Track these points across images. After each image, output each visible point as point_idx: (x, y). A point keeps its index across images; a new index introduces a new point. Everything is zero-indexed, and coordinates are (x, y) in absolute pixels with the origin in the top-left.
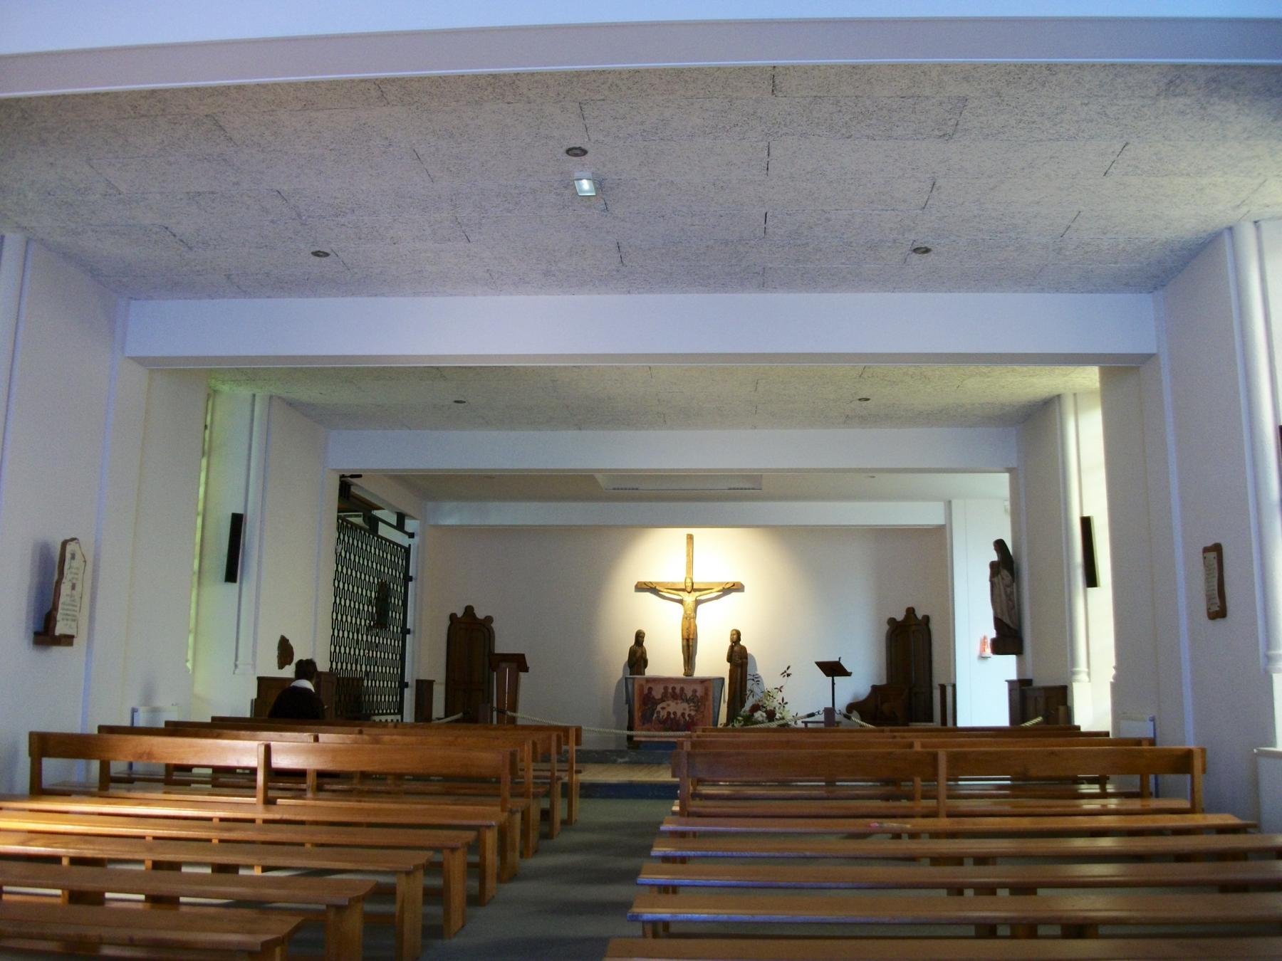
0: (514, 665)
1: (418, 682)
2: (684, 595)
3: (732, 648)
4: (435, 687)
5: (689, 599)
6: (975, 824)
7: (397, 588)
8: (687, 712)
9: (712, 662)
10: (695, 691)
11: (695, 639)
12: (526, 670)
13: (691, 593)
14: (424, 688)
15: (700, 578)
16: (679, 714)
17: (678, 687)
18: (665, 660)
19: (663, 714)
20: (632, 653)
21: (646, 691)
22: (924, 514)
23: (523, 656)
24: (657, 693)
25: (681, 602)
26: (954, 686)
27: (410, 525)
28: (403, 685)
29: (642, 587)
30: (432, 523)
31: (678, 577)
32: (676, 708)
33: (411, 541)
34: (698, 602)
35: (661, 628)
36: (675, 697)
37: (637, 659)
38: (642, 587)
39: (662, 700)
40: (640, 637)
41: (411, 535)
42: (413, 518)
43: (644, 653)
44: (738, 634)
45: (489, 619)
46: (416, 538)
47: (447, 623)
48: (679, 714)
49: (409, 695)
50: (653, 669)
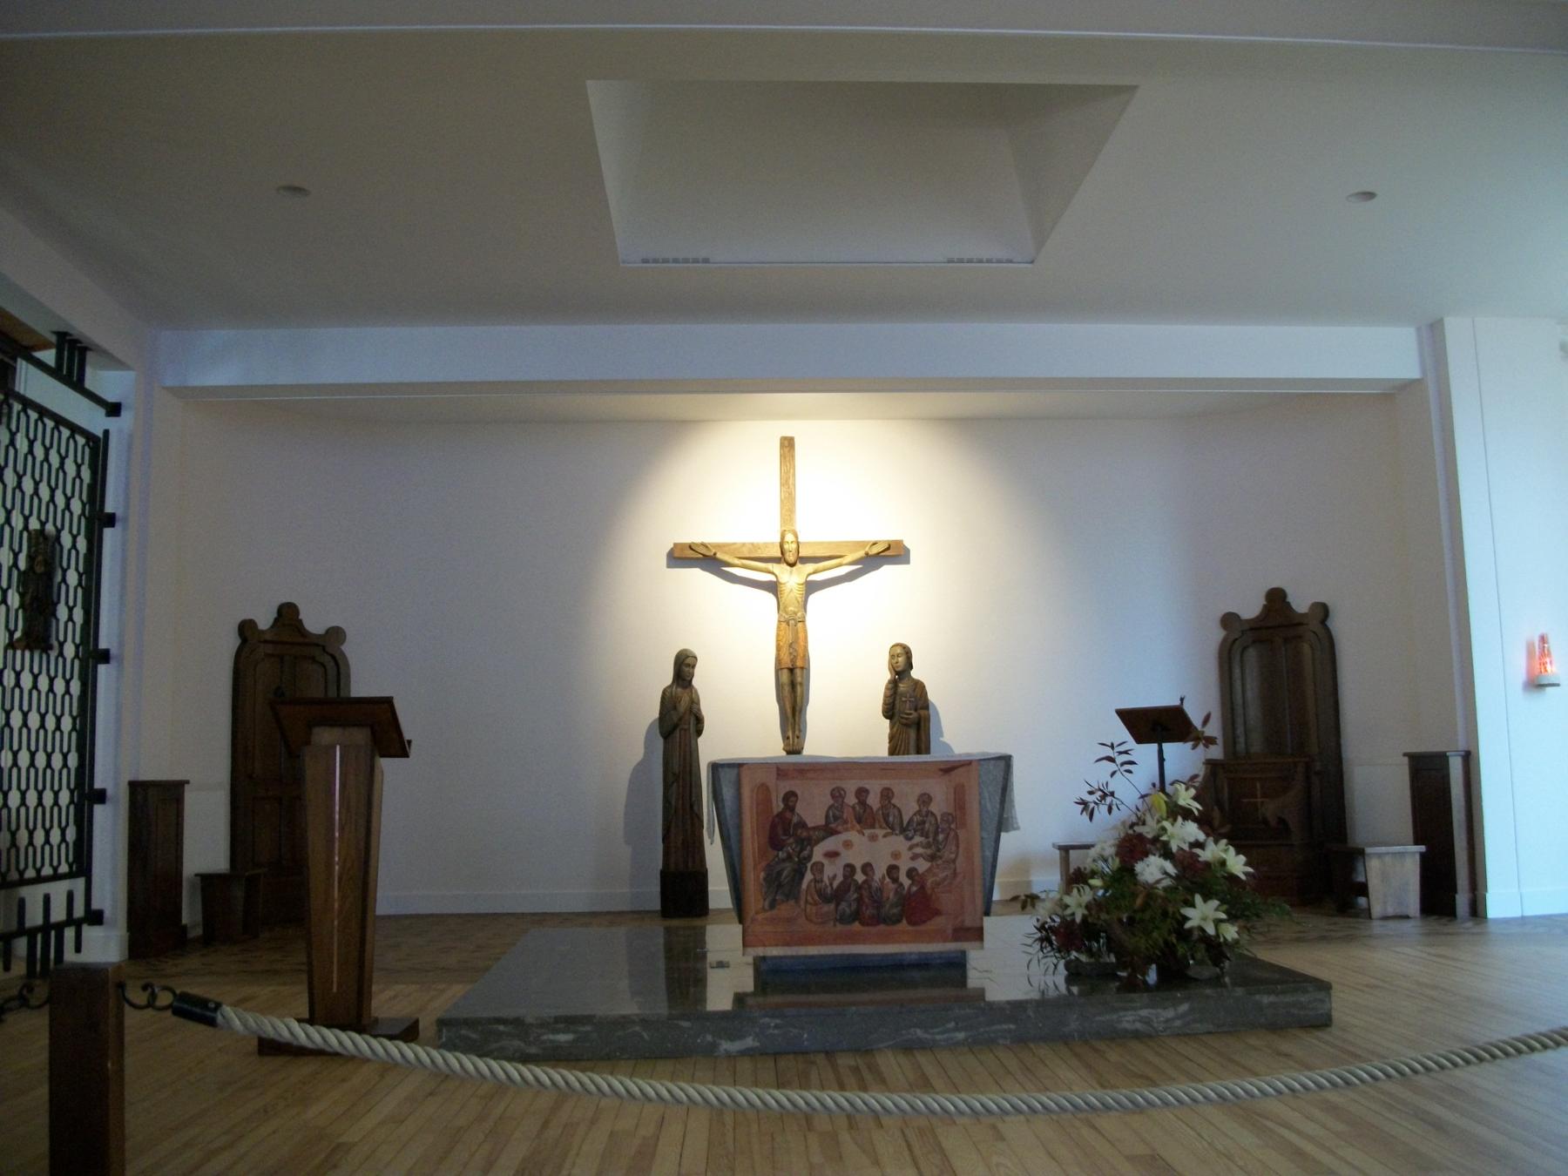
0: (360, 736)
1: (134, 785)
2: (782, 573)
3: (893, 685)
4: (190, 798)
5: (792, 579)
6: (711, 836)
7: (72, 542)
8: (904, 865)
9: (845, 721)
10: (925, 799)
11: (805, 669)
12: (400, 749)
13: (790, 569)
14: (156, 806)
15: (813, 531)
16: (880, 871)
17: (875, 787)
18: (739, 724)
19: (833, 872)
20: (669, 703)
21: (778, 806)
22: (1378, 353)
23: (388, 701)
24: (812, 811)
25: (773, 588)
26: (1470, 760)
27: (100, 379)
28: (88, 796)
29: (683, 557)
30: (169, 383)
31: (763, 532)
32: (872, 852)
33: (112, 424)
34: (811, 587)
35: (732, 646)
36: (865, 818)
37: (680, 718)
38: (683, 557)
39: (828, 831)
40: (684, 666)
41: (114, 410)
42: (119, 364)
43: (694, 702)
44: (908, 653)
45: (336, 634)
46: (126, 419)
47: (233, 642)
48: (880, 871)
49: (110, 826)
50: (711, 748)
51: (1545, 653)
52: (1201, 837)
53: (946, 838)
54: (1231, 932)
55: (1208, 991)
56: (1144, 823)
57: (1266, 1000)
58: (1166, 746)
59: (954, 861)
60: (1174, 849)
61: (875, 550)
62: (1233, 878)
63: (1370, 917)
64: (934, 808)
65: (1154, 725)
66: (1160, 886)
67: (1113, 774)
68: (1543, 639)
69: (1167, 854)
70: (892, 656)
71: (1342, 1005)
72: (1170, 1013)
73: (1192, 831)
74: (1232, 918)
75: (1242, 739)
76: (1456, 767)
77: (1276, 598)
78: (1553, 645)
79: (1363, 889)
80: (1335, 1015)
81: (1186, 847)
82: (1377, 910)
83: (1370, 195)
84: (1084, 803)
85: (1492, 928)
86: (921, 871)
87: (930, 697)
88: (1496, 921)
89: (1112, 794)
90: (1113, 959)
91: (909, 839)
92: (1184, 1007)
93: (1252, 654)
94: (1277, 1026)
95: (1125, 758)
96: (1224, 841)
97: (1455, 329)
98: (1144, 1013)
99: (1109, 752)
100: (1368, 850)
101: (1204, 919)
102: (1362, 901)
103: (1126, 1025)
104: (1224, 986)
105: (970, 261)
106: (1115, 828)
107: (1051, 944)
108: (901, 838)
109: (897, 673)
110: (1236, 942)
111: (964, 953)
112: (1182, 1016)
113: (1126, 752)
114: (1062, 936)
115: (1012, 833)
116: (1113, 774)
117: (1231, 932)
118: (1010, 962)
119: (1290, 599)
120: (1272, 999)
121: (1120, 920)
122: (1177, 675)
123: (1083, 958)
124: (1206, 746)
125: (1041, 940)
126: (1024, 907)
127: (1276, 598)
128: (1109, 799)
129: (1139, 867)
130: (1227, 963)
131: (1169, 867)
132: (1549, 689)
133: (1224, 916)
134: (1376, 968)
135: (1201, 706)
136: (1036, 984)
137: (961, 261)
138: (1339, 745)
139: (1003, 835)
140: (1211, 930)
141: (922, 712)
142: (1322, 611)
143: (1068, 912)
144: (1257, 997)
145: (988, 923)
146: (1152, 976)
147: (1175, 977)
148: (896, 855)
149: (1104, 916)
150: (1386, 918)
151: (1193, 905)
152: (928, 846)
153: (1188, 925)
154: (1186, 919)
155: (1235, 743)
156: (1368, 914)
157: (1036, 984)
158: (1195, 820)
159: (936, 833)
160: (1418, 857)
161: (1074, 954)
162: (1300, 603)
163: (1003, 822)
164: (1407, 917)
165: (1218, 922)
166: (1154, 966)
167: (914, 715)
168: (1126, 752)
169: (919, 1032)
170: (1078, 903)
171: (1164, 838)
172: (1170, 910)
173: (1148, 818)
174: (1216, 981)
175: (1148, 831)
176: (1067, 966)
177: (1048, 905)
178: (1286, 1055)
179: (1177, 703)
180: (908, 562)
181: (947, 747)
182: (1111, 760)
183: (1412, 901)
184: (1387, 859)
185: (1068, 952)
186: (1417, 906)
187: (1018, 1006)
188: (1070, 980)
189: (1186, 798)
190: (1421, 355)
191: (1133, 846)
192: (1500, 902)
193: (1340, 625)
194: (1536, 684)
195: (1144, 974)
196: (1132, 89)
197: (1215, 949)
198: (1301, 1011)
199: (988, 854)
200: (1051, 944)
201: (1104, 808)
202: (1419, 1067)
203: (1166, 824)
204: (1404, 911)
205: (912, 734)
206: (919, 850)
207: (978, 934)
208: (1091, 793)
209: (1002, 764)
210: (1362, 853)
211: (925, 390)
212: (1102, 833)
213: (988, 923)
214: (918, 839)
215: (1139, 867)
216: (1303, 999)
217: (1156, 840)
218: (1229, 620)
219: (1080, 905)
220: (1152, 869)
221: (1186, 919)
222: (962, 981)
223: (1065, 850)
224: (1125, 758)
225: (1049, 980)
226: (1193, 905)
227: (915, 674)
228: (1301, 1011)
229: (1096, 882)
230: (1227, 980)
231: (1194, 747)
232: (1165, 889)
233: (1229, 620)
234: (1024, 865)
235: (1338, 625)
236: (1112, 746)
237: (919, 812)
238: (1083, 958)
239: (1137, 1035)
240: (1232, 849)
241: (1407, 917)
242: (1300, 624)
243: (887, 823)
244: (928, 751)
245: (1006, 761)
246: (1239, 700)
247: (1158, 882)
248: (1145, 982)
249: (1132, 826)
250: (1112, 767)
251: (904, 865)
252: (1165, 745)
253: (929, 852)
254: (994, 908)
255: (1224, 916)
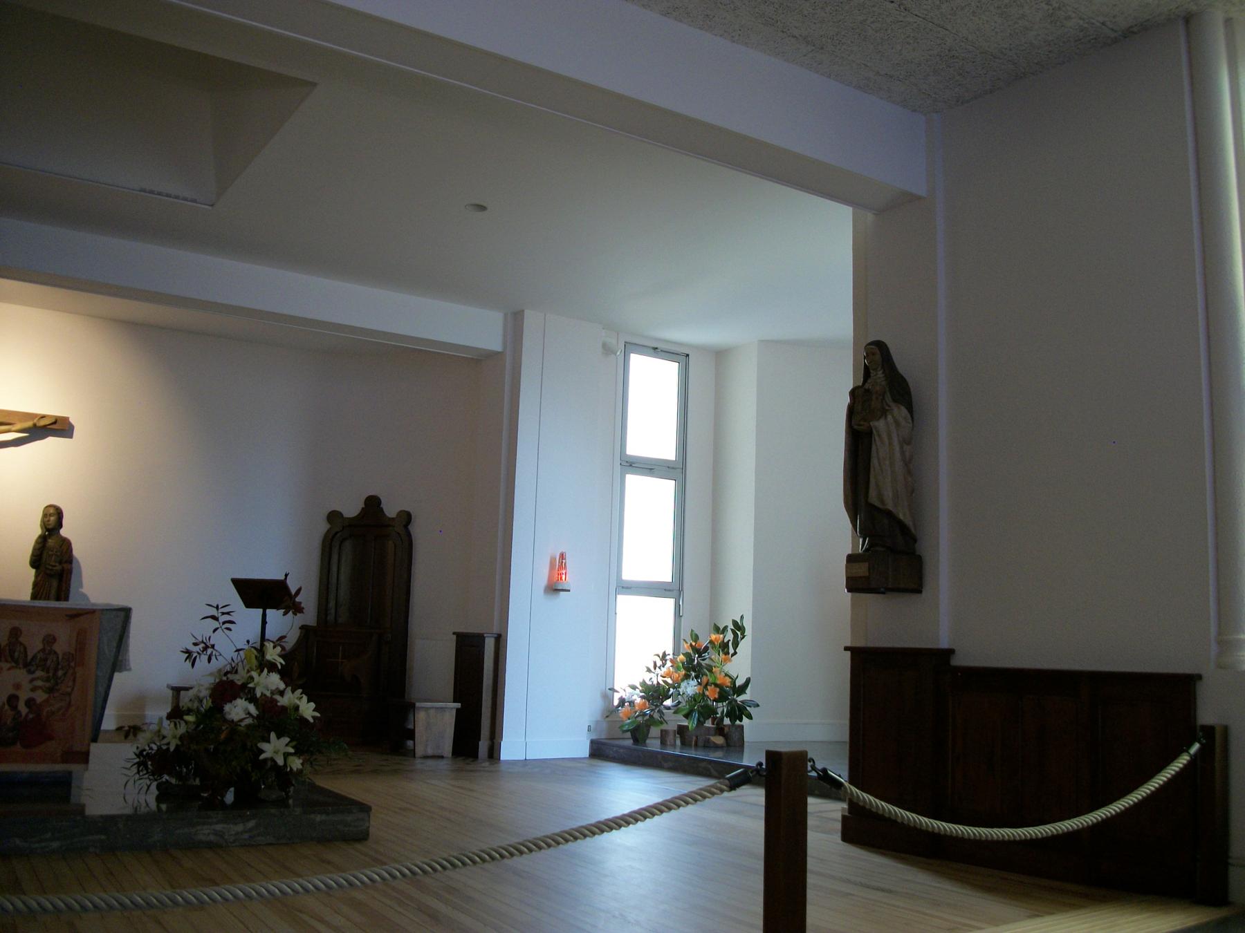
3: (42, 542)
8: (24, 696)
10: (50, 640)
22: (477, 329)
26: (500, 641)
44: (59, 513)
51: (562, 566)
52: (282, 686)
53: (65, 674)
54: (296, 763)
55: (273, 811)
56: (236, 672)
57: (319, 818)
58: (270, 613)
59: (70, 694)
60: (258, 695)
61: (43, 423)
62: (303, 720)
63: (414, 756)
64: (56, 647)
65: (259, 593)
66: (243, 724)
67: (215, 630)
68: (562, 556)
69: (252, 699)
70: (45, 515)
71: (376, 824)
72: (240, 828)
73: (275, 680)
74: (298, 753)
75: (333, 611)
76: (489, 644)
77: (373, 503)
78: (569, 561)
79: (411, 735)
80: (372, 830)
81: (268, 694)
82: (420, 751)
83: (482, 208)
84: (188, 653)
85: (503, 768)
86: (39, 701)
87: (75, 552)
88: (507, 762)
89: (213, 646)
90: (197, 782)
91: (30, 672)
92: (251, 824)
93: (348, 545)
94: (328, 838)
95: (227, 618)
96: (300, 691)
97: (532, 319)
98: (219, 827)
99: (214, 612)
100: (418, 704)
101: (276, 752)
102: (410, 743)
103: (203, 838)
104: (287, 806)
105: (159, 194)
106: (211, 674)
107: (147, 768)
108: (24, 671)
109: (48, 530)
110: (300, 772)
111: (70, 773)
112: (250, 830)
113: (228, 613)
114: (154, 762)
115: (125, 674)
116: (215, 630)
117: (296, 763)
118: (111, 783)
119: (384, 506)
120: (324, 817)
121: (207, 750)
122: (284, 554)
123: (173, 781)
124: (295, 614)
125: (139, 764)
126: (126, 736)
127: (373, 503)
128: (209, 651)
129: (227, 707)
130: (292, 789)
131: (252, 709)
132: (562, 593)
133: (292, 751)
134: (412, 800)
135: (303, 579)
136: (130, 801)
137: (152, 192)
138: (407, 622)
139: (117, 676)
140: (280, 762)
141: (65, 566)
142: (406, 518)
143: (165, 741)
144: (312, 816)
145: (94, 748)
146: (230, 797)
147: (249, 800)
148: (18, 686)
149: (194, 747)
150: (426, 757)
151: (269, 741)
152: (48, 680)
153: (262, 757)
154: (262, 752)
155: (326, 615)
156: (412, 753)
157: (130, 801)
158: (279, 672)
159: (56, 670)
160: (454, 712)
161: (166, 777)
162: (391, 509)
163: (118, 663)
164: (442, 757)
165: (286, 755)
166: (232, 789)
167: (58, 568)
168: (228, 613)
169: (18, 841)
170: (172, 734)
171: (251, 685)
172: (249, 744)
173: (240, 669)
174: (282, 803)
175: (238, 679)
176: (158, 787)
177: (148, 735)
178: (329, 863)
179: (282, 578)
180: (71, 436)
181: (85, 596)
182: (215, 618)
183: (447, 747)
184: (432, 712)
185: (161, 775)
186: (451, 749)
187: (112, 819)
188: (159, 799)
189: (273, 654)
190: (505, 336)
191: (225, 689)
192: (510, 749)
193: (419, 531)
194: (554, 589)
195: (223, 796)
196: (314, 85)
197: (283, 776)
198: (344, 827)
199: (101, 690)
200: (147, 768)
201: (205, 658)
202: (407, 872)
203: (254, 674)
204: (439, 752)
205: (55, 583)
206: (39, 683)
207: (84, 758)
208: (195, 644)
209: (122, 614)
210: (413, 706)
211: (115, 295)
212: (202, 676)
213: (94, 748)
214: (39, 673)
215: (227, 707)
216: (349, 818)
217: (244, 686)
218: (333, 516)
219: (174, 737)
220: (239, 710)
221: (262, 752)
222: (66, 798)
223: (177, 690)
224: (227, 618)
225: (142, 798)
226: (269, 741)
227: (63, 532)
228: (344, 827)
229: (190, 718)
230: (291, 801)
231: (285, 614)
232: (248, 726)
233: (333, 516)
234: (140, 701)
235: (417, 530)
236: (217, 607)
237: (43, 650)
238: (173, 781)
239: (211, 846)
240: (305, 698)
241: (442, 757)
242: (388, 526)
243: (12, 657)
244: (67, 599)
245: (126, 613)
246: (334, 580)
247: (241, 720)
248: (223, 802)
249: (226, 674)
250: (216, 624)
251: (24, 696)
252: (268, 611)
253: (48, 685)
254: (101, 737)
255: (292, 751)
